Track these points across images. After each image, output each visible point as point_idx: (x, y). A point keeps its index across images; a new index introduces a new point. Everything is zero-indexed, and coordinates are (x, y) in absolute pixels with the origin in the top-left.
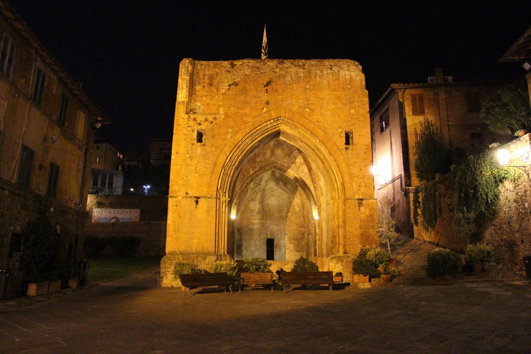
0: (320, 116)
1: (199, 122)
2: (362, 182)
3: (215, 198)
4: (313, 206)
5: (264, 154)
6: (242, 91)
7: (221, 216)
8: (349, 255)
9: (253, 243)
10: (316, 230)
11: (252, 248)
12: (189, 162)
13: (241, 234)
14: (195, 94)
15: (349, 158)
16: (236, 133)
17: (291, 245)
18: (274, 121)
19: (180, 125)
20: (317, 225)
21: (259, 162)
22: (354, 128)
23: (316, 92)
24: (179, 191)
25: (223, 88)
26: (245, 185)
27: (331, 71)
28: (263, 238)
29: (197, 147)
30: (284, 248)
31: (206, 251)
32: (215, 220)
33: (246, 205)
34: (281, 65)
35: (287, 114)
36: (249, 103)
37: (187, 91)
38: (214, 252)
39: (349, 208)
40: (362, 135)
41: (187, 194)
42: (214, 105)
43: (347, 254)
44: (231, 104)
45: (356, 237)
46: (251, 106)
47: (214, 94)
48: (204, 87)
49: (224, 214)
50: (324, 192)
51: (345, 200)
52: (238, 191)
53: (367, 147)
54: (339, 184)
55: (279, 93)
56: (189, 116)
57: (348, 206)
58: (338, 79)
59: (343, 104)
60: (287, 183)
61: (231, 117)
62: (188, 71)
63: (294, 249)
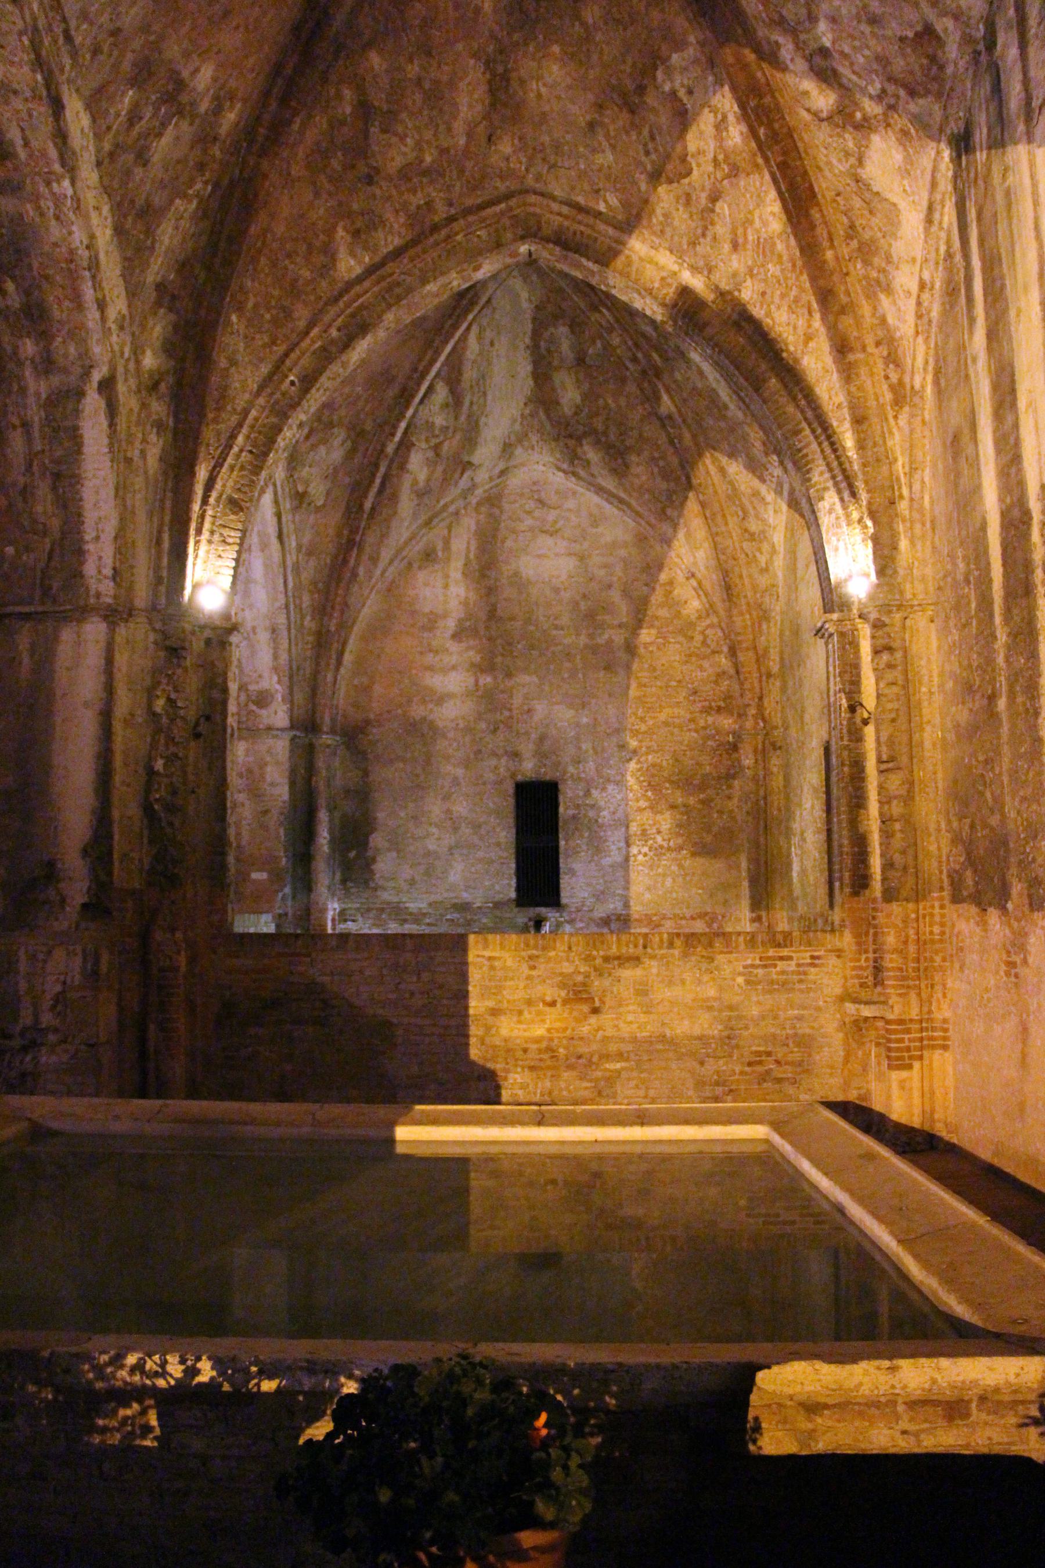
4: (829, 505)
9: (435, 809)
11: (428, 835)
17: (659, 817)
21: (405, 174)
26: (303, 361)
28: (490, 776)
30: (620, 833)
50: (922, 380)
52: (251, 404)
60: (629, 449)
63: (680, 841)
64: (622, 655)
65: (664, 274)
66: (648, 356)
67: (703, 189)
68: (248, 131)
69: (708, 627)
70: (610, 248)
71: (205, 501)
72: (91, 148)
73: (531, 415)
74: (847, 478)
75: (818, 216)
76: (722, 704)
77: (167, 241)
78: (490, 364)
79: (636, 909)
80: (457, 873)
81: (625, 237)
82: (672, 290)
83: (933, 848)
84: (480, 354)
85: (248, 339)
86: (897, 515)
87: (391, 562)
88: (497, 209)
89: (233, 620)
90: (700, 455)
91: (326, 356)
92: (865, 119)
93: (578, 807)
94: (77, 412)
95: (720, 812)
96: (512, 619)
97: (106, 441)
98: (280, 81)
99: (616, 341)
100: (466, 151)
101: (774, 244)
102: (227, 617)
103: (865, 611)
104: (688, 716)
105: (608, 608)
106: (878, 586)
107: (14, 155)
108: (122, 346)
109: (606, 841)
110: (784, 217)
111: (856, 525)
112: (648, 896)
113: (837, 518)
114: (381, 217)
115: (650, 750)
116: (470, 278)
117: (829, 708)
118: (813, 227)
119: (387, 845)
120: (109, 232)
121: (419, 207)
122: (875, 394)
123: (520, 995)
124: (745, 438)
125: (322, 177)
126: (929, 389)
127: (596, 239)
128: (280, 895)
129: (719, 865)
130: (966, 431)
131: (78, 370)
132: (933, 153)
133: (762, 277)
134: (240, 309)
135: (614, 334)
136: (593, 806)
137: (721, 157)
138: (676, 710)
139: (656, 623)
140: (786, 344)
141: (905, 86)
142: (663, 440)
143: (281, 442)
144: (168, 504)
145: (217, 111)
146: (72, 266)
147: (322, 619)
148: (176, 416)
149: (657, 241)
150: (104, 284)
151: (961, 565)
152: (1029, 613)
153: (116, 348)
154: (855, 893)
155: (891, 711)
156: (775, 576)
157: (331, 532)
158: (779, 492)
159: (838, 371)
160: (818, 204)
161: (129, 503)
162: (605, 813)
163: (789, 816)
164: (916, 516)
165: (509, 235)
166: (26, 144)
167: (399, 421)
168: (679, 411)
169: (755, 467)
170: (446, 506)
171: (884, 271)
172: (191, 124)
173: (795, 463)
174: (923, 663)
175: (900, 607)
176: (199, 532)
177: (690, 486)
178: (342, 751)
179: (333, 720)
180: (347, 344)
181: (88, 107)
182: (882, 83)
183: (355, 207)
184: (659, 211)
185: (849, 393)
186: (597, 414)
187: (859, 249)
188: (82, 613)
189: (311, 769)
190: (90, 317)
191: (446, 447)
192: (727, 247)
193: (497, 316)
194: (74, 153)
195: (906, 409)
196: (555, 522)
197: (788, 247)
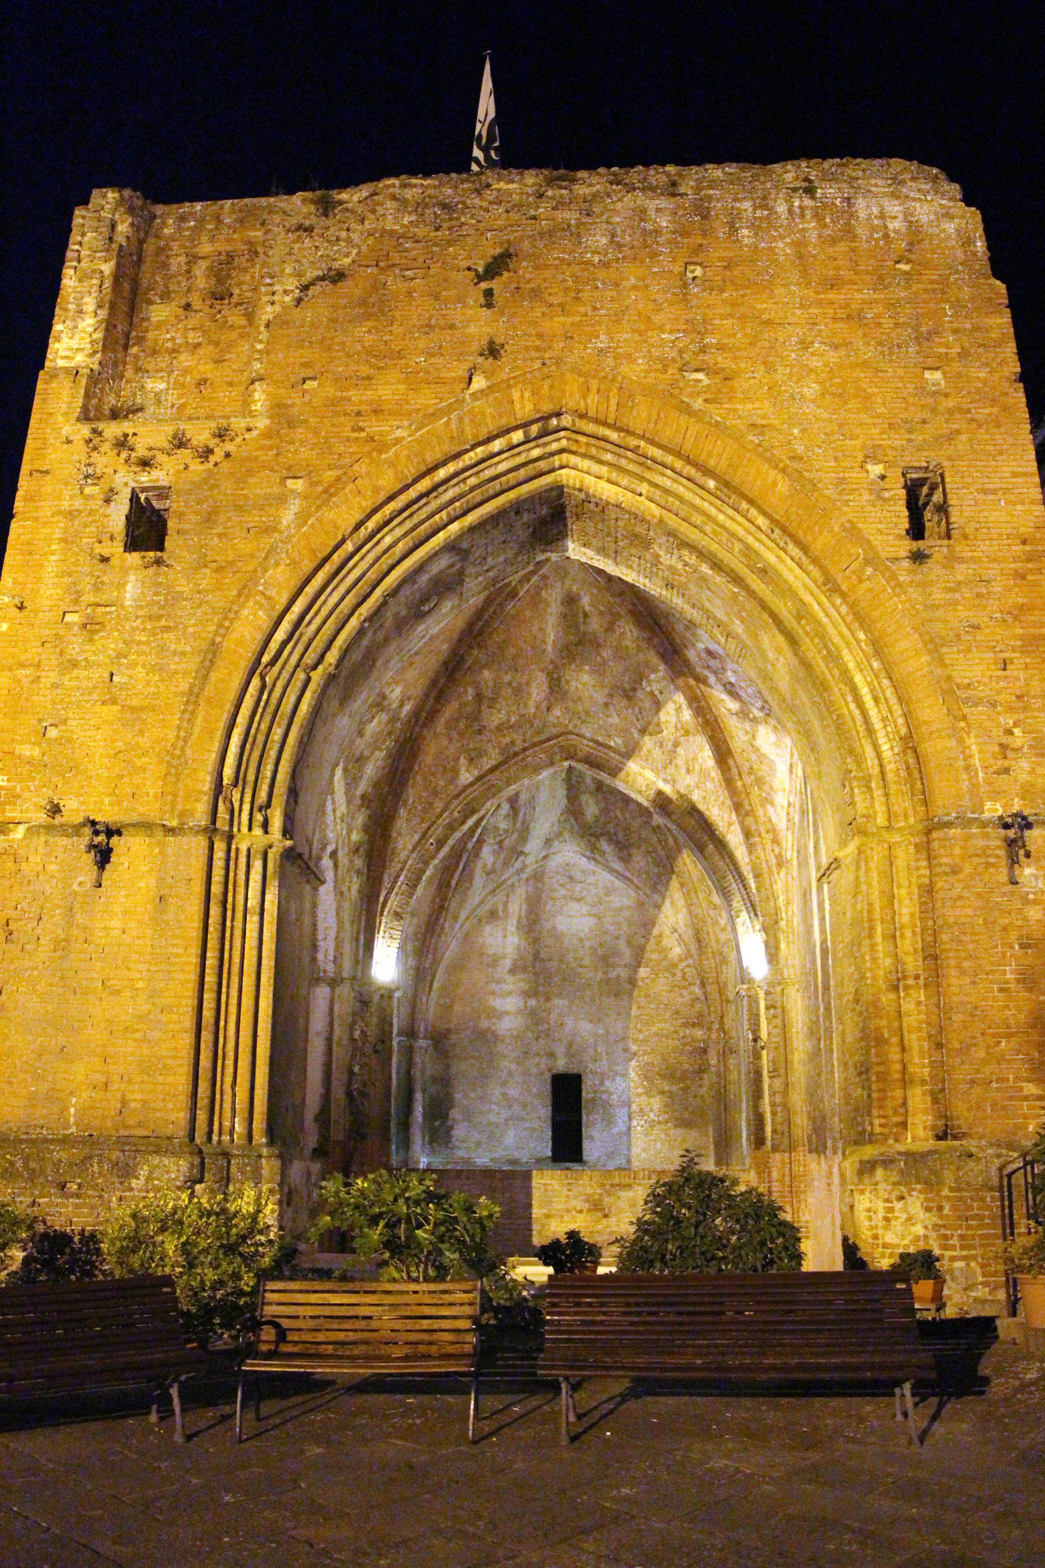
0: (766, 404)
1: (141, 452)
2: (1016, 731)
3: (205, 830)
5: (519, 691)
6: (363, 303)
7: (238, 933)
8: (971, 1144)
9: (496, 1092)
10: (757, 1025)
12: (76, 647)
13: (448, 1057)
14: (140, 340)
15: (935, 607)
16: (328, 494)
17: (652, 1100)
18: (526, 434)
19: (47, 472)
21: (499, 728)
22: (950, 458)
23: (743, 296)
24: (18, 796)
25: (276, 298)
26: (438, 831)
27: (808, 202)
29: (125, 571)
30: (625, 1110)
31: (140, 1125)
32: (195, 950)
34: (561, 188)
35: (593, 399)
36: (399, 355)
37: (100, 322)
38: (182, 1133)
39: (955, 871)
40: (994, 492)
41: (55, 810)
42: (231, 384)
43: (955, 1137)
44: (305, 365)
45: (1008, 1036)
46: (407, 366)
47: (234, 335)
48: (187, 307)
49: (253, 921)
50: (790, 854)
51: (928, 832)
52: (408, 857)
53: (1028, 548)
54: (885, 747)
55: (551, 305)
56: (94, 431)
57: (945, 860)
58: (849, 233)
59: (881, 344)
61: (305, 421)
62: (111, 239)
64: (628, 986)
68: (416, 713)
69: (688, 966)
74: (752, 905)
79: (636, 1164)
80: (510, 1138)
83: (799, 1122)
85: (408, 820)
87: (468, 918)
90: (679, 851)
91: (451, 828)
93: (595, 1092)
95: (695, 1096)
105: (616, 953)
112: (644, 1155)
115: (645, 1053)
118: (729, 769)
123: (561, 1206)
126: (795, 861)
142: (654, 840)
145: (402, 705)
162: (614, 1097)
165: (558, 758)
170: (505, 881)
175: (779, 984)
177: (673, 872)
178: (431, 1050)
179: (426, 1029)
188: (317, 981)
191: (506, 842)
192: (683, 771)
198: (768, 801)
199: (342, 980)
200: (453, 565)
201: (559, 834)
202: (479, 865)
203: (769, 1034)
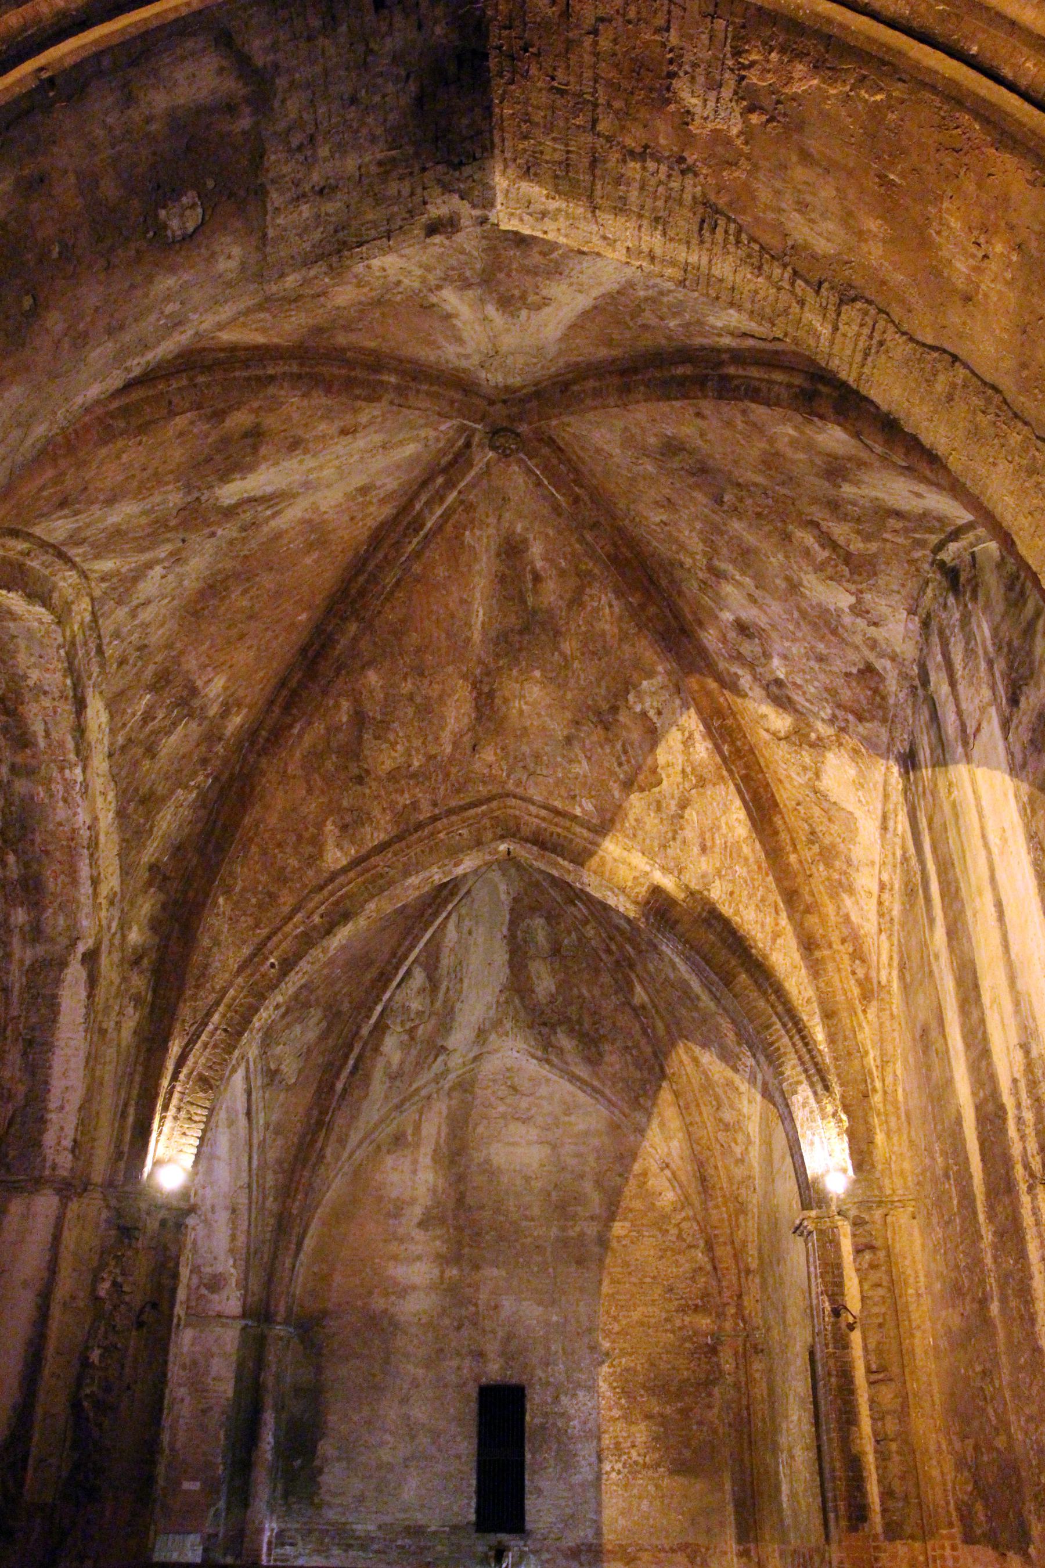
4: (803, 1097)
9: (391, 1412)
11: (382, 1444)
13: (320, 1354)
20: (847, 1246)
21: (393, 776)
26: (284, 945)
28: (452, 1378)
33: (358, 1175)
50: (888, 975)
52: (230, 984)
64: (596, 1249)
65: (637, 874)
66: (621, 948)
67: (673, 798)
68: (251, 734)
69: (684, 1219)
70: (585, 849)
71: (175, 1077)
72: (106, 742)
73: (507, 1002)
74: (819, 1071)
75: (780, 822)
76: (700, 1303)
77: (164, 825)
78: (467, 950)
79: (609, 1538)
80: (411, 1489)
81: (599, 839)
82: (645, 889)
83: (935, 1473)
84: (459, 942)
86: (871, 1108)
87: (361, 1143)
88: (479, 810)
89: (192, 1201)
90: (673, 1045)
91: (308, 941)
92: (819, 738)
93: (546, 1415)
94: (58, 982)
95: (700, 1423)
96: (482, 1207)
97: (83, 1011)
98: (285, 692)
99: (590, 932)
100: (451, 759)
101: (740, 849)
102: (185, 1194)
103: (844, 1208)
104: (664, 1315)
105: (579, 1199)
106: (856, 1182)
107: (35, 745)
108: (110, 921)
109: (575, 1455)
110: (749, 823)
111: (831, 1119)
112: (622, 1522)
113: (812, 1112)
114: (368, 814)
115: (623, 1353)
116: (450, 872)
117: (811, 1311)
118: (776, 833)
119: (336, 1453)
120: (111, 815)
121: (405, 806)
122: (843, 989)
124: (717, 1028)
125: (316, 776)
126: (895, 985)
127: (571, 841)
128: (212, 1510)
129: (699, 1486)
130: (934, 1025)
131: (64, 941)
132: (883, 769)
133: (730, 877)
134: (228, 891)
135: (588, 927)
136: (563, 1415)
137: (688, 770)
138: (650, 1309)
139: (630, 1215)
140: (755, 941)
141: (854, 712)
143: (256, 1023)
144: (137, 1078)
145: (225, 713)
146: (73, 844)
147: (284, 1202)
148: (155, 991)
149: (630, 843)
150: (100, 862)
151: (940, 1160)
152: (1014, 1211)
153: (104, 922)
154: (853, 1528)
155: (877, 1315)
156: (751, 1167)
157: (301, 1110)
158: (752, 1081)
159: (807, 967)
160: (781, 813)
161: (98, 1073)
162: (575, 1422)
163: (776, 1431)
164: (890, 1108)
165: (490, 835)
166: (47, 734)
167: (376, 1003)
168: (652, 1001)
169: (727, 1057)
170: (417, 1090)
171: (845, 873)
172: (199, 725)
173: (767, 1057)
174: (907, 1262)
176: (166, 1108)
179: (289, 1311)
180: (329, 930)
181: (108, 706)
182: (832, 708)
183: (345, 803)
184: (631, 817)
185: (818, 988)
186: (571, 1004)
187: (821, 854)
188: (38, 1183)
189: (260, 1363)
190: (83, 891)
191: (420, 1031)
192: (696, 850)
193: (476, 906)
194: (89, 744)
195: (874, 1003)
196: (529, 1109)
197: (753, 850)
198: (842, 886)
199: (86, 1187)
200: (230, 109)
201: (498, 1023)
202: (380, 1064)
203: (863, 1299)
